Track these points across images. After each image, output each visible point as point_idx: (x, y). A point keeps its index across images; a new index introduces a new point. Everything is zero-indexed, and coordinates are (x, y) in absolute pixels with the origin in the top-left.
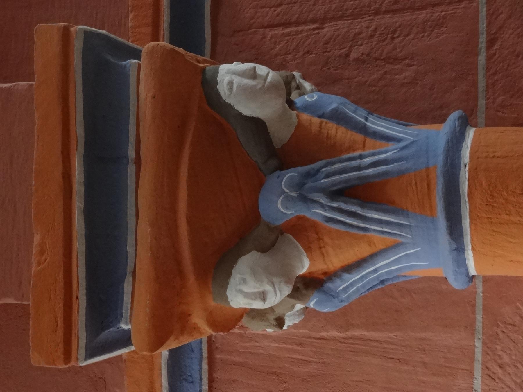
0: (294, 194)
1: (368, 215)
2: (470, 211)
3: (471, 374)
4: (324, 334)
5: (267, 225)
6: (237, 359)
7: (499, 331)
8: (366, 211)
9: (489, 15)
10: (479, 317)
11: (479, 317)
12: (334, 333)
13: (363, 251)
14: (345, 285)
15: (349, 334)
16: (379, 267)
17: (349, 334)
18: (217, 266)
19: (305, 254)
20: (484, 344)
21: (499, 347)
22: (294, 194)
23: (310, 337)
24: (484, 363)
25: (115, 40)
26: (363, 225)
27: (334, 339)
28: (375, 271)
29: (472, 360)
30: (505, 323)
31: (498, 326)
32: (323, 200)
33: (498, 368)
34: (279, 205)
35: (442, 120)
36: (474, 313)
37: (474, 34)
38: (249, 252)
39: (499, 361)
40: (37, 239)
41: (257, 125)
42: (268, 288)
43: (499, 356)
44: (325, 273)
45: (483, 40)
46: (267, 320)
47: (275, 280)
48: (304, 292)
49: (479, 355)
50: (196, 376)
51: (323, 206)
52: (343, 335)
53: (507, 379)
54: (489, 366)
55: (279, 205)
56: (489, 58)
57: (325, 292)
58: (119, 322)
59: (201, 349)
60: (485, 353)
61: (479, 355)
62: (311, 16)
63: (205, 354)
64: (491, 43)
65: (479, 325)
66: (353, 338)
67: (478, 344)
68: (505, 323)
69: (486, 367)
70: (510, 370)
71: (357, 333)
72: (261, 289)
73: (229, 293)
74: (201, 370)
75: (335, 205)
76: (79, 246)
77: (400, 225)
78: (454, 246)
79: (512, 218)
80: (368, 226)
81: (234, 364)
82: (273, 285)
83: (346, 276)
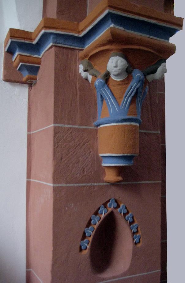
0: (141, 79)
1: (129, 98)
2: (128, 125)
3: (69, 124)
4: (77, 83)
5: (132, 71)
6: (69, 56)
7: (80, 132)
8: (131, 97)
9: (150, 133)
10: (84, 127)
11: (84, 127)
12: (78, 86)
13: (117, 96)
14: (106, 90)
15: (78, 90)
16: (111, 100)
17: (78, 90)
18: (125, 54)
19: (122, 80)
20: (77, 128)
21: (76, 132)
22: (141, 79)
23: (76, 79)
24: (72, 128)
25: (104, 33)
26: (127, 96)
27: (76, 86)
28: (110, 99)
29: (73, 124)
30: (82, 134)
31: (82, 132)
32: (138, 86)
33: (70, 132)
34: (138, 74)
35: (141, 118)
36: (85, 126)
37: (147, 129)
38: (128, 64)
39: (72, 132)
40: (138, 5)
41: (154, 71)
42: (118, 68)
43: (74, 132)
44: (108, 85)
45: (146, 131)
46: (87, 67)
47: (120, 71)
48: (105, 78)
49: (74, 126)
50: (66, 43)
51: (136, 86)
52: (78, 88)
53: (68, 134)
54: (71, 129)
55: (138, 74)
56: (142, 133)
57: (104, 84)
58: (114, 24)
59: (73, 46)
60: (75, 128)
61: (74, 126)
62: (150, 89)
63: (72, 47)
64: (145, 133)
65: (82, 127)
66: (77, 92)
67: (77, 127)
68: (82, 134)
69: (71, 128)
70: (70, 135)
71: (78, 93)
72: (118, 66)
73: (117, 58)
74: (68, 45)
75: (135, 89)
76: (137, 17)
77: (125, 106)
78: (119, 120)
79: (126, 135)
80: (126, 98)
81: (68, 55)
82: (119, 70)
83: (109, 91)
